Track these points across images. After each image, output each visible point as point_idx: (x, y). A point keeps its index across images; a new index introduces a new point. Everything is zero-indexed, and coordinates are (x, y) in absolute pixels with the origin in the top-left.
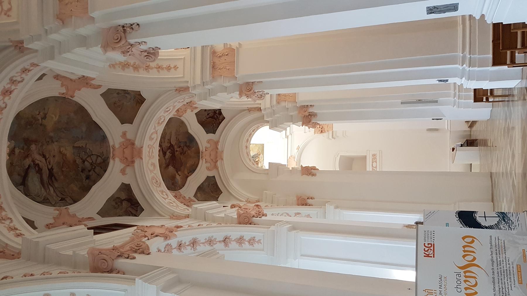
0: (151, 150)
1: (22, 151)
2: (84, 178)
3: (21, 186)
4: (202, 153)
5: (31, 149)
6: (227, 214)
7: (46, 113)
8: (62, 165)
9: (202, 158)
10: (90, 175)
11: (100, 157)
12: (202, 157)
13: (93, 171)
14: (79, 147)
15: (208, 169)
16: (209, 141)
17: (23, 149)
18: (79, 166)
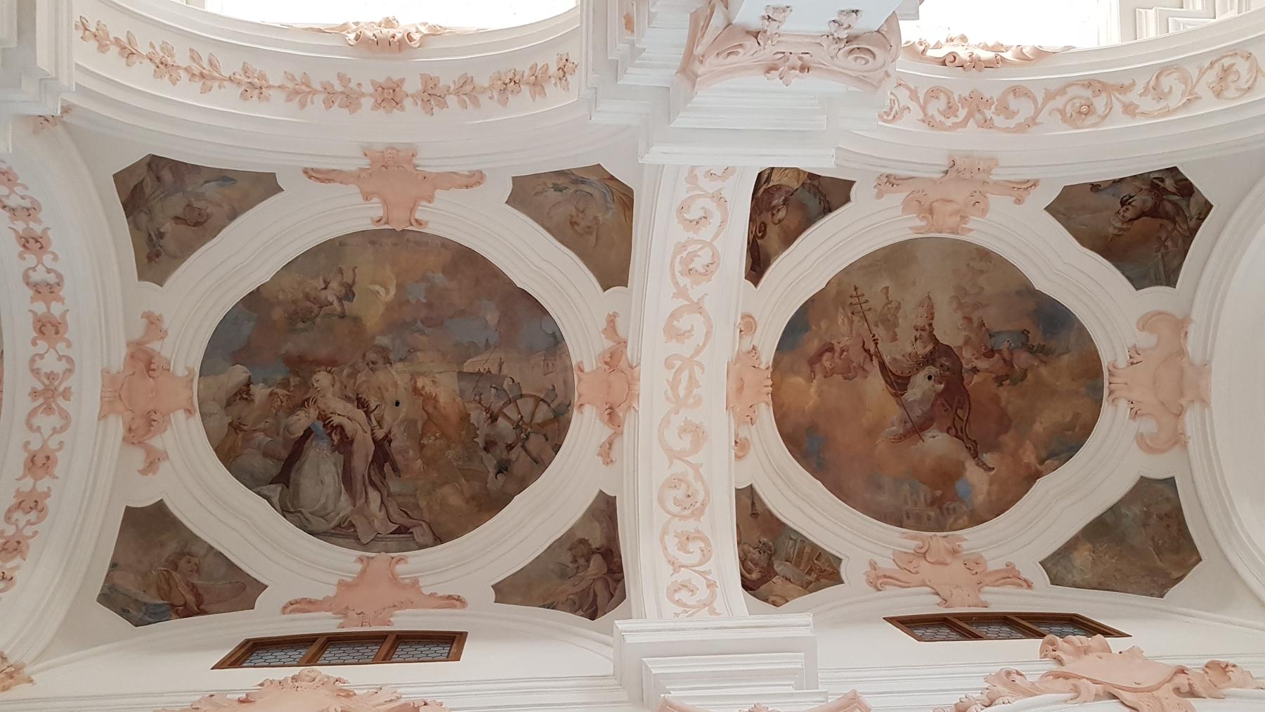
0: (685, 376)
1: (281, 391)
2: (491, 470)
3: (273, 486)
4: (1111, 374)
5: (316, 385)
6: (764, 704)
7: (350, 281)
8: (422, 430)
9: (1112, 397)
10: (509, 461)
11: (545, 402)
12: (1111, 392)
13: (520, 449)
14: (479, 373)
15: (1147, 445)
16: (1146, 323)
17: (285, 384)
18: (478, 432)
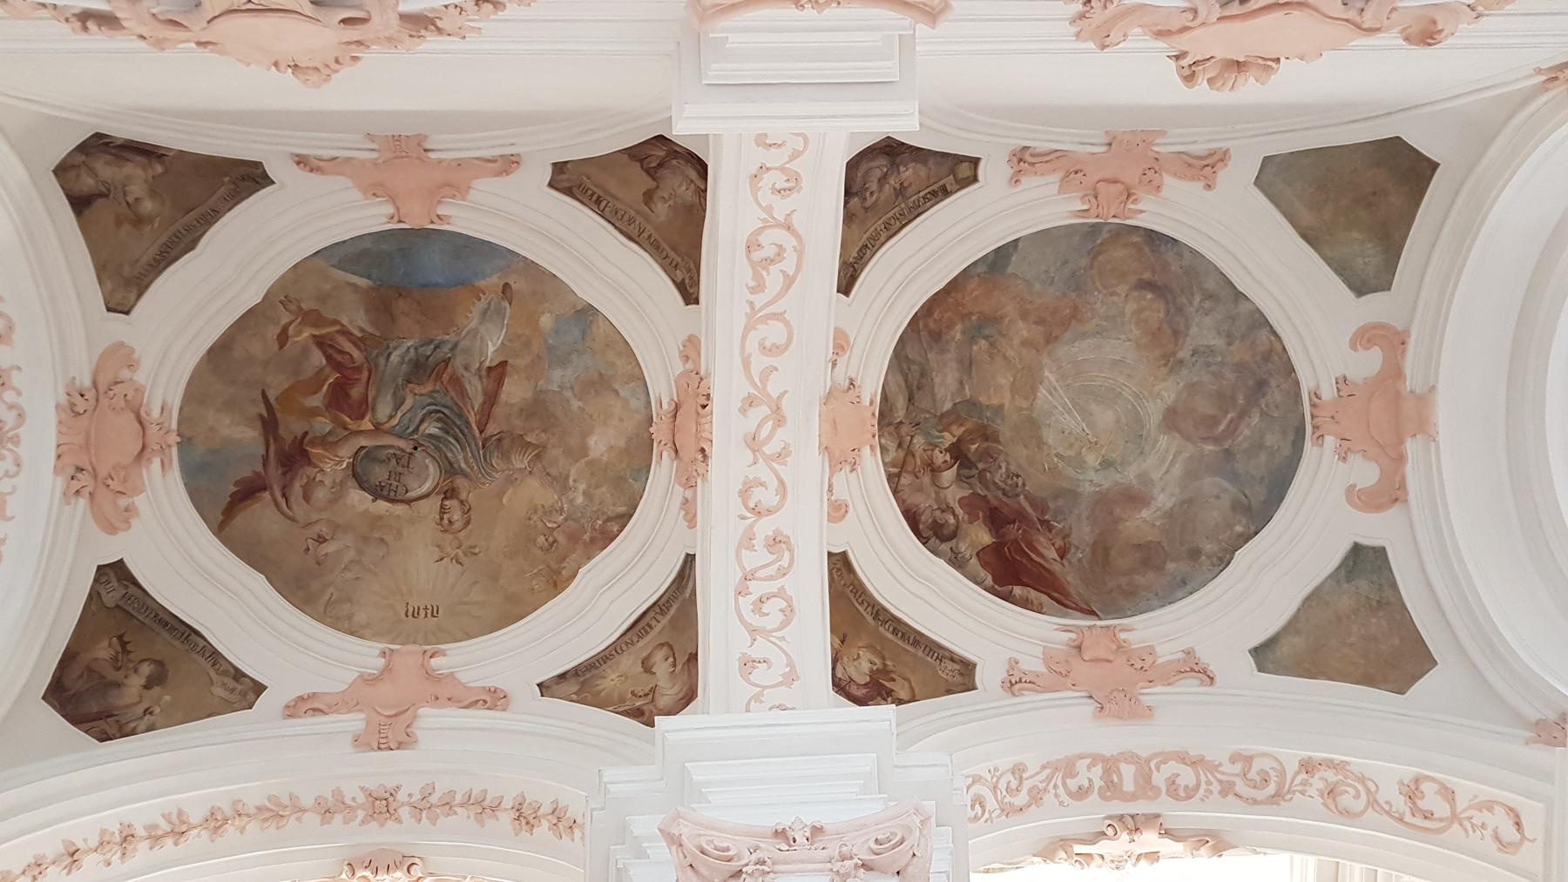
16: (1366, 337)
